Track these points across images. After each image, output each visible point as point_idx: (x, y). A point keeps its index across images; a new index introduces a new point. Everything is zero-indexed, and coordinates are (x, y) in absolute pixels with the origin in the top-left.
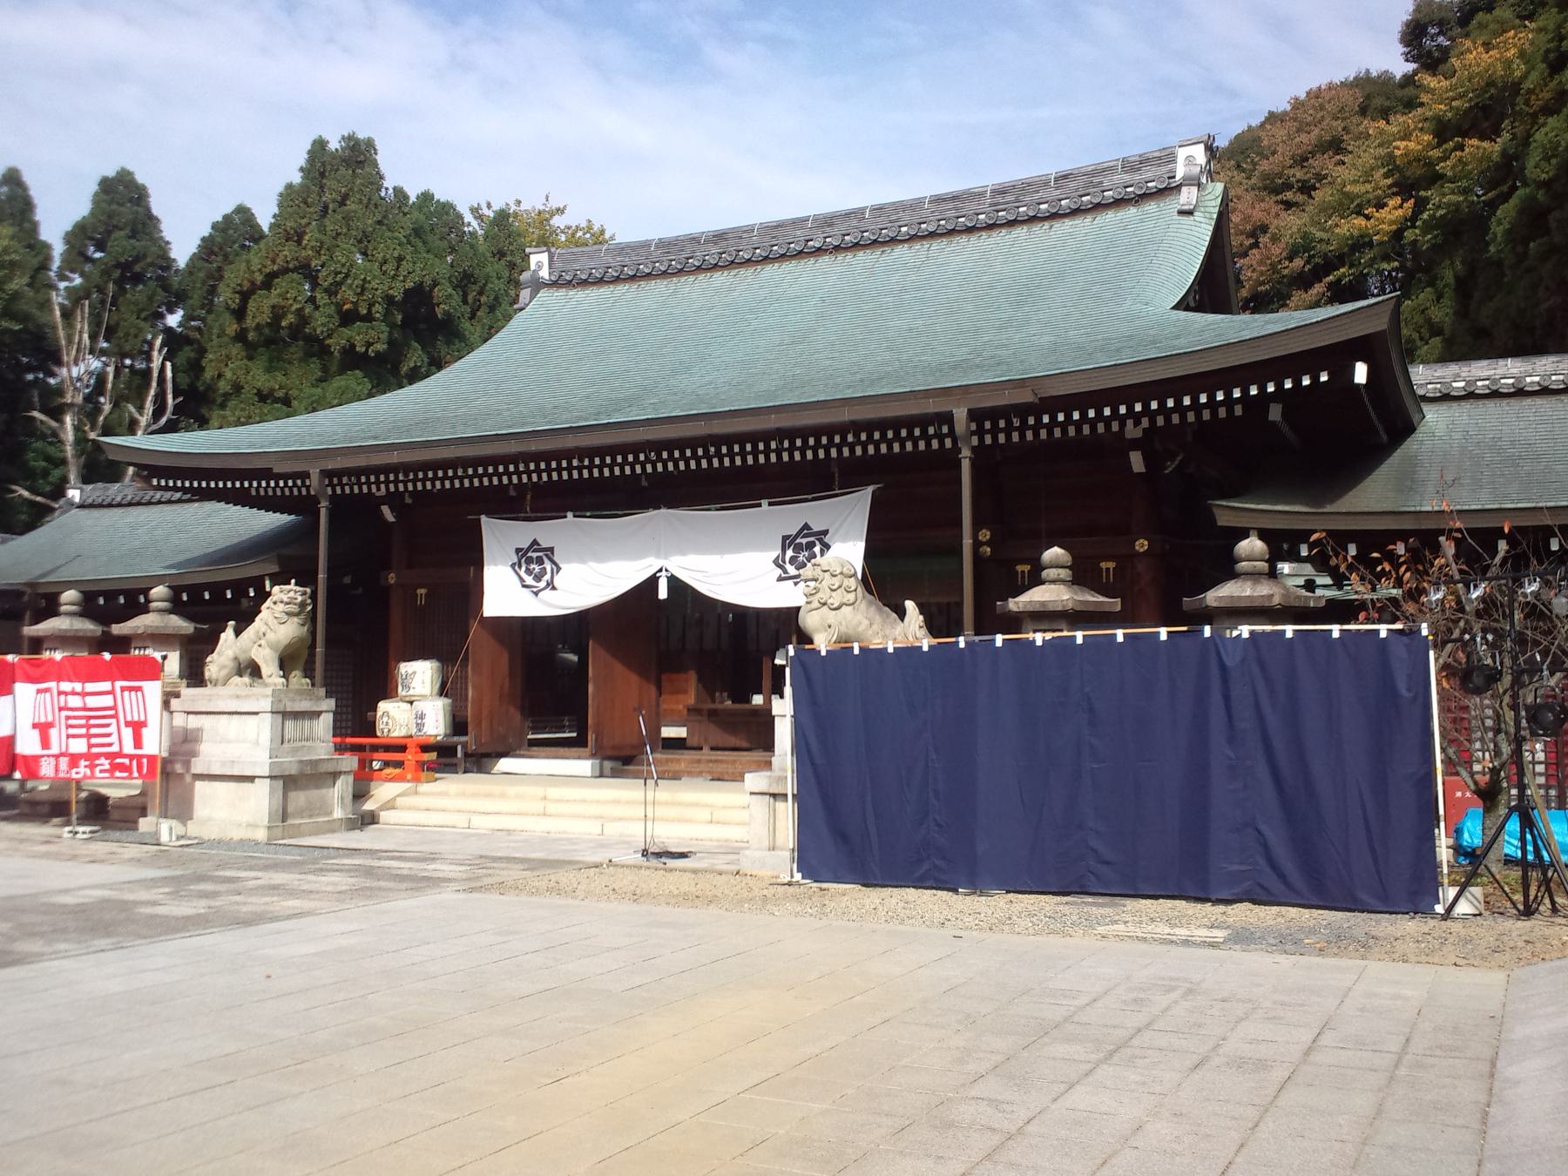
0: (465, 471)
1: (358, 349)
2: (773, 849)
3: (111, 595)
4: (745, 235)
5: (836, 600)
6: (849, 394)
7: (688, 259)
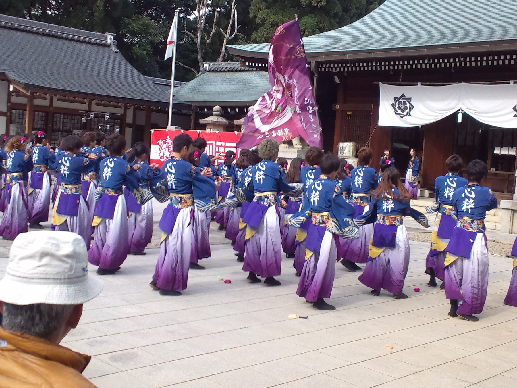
1: (313, 4)
2: (511, 233)
3: (233, 108)
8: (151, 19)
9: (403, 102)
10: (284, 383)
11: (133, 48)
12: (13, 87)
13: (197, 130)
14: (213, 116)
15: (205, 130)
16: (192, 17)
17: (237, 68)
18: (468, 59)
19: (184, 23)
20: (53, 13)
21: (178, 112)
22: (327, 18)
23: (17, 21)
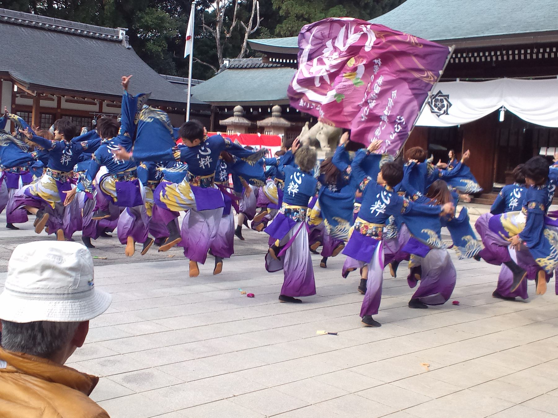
0: (468, 54)
3: (256, 108)
8: (165, 12)
9: (440, 99)
10: (312, 405)
11: (147, 44)
12: (18, 87)
13: (217, 132)
14: (233, 116)
15: (226, 132)
16: (210, 10)
17: (260, 65)
18: (510, 52)
19: (201, 16)
20: (60, 7)
21: (196, 113)
22: (357, 10)
23: (21, 16)
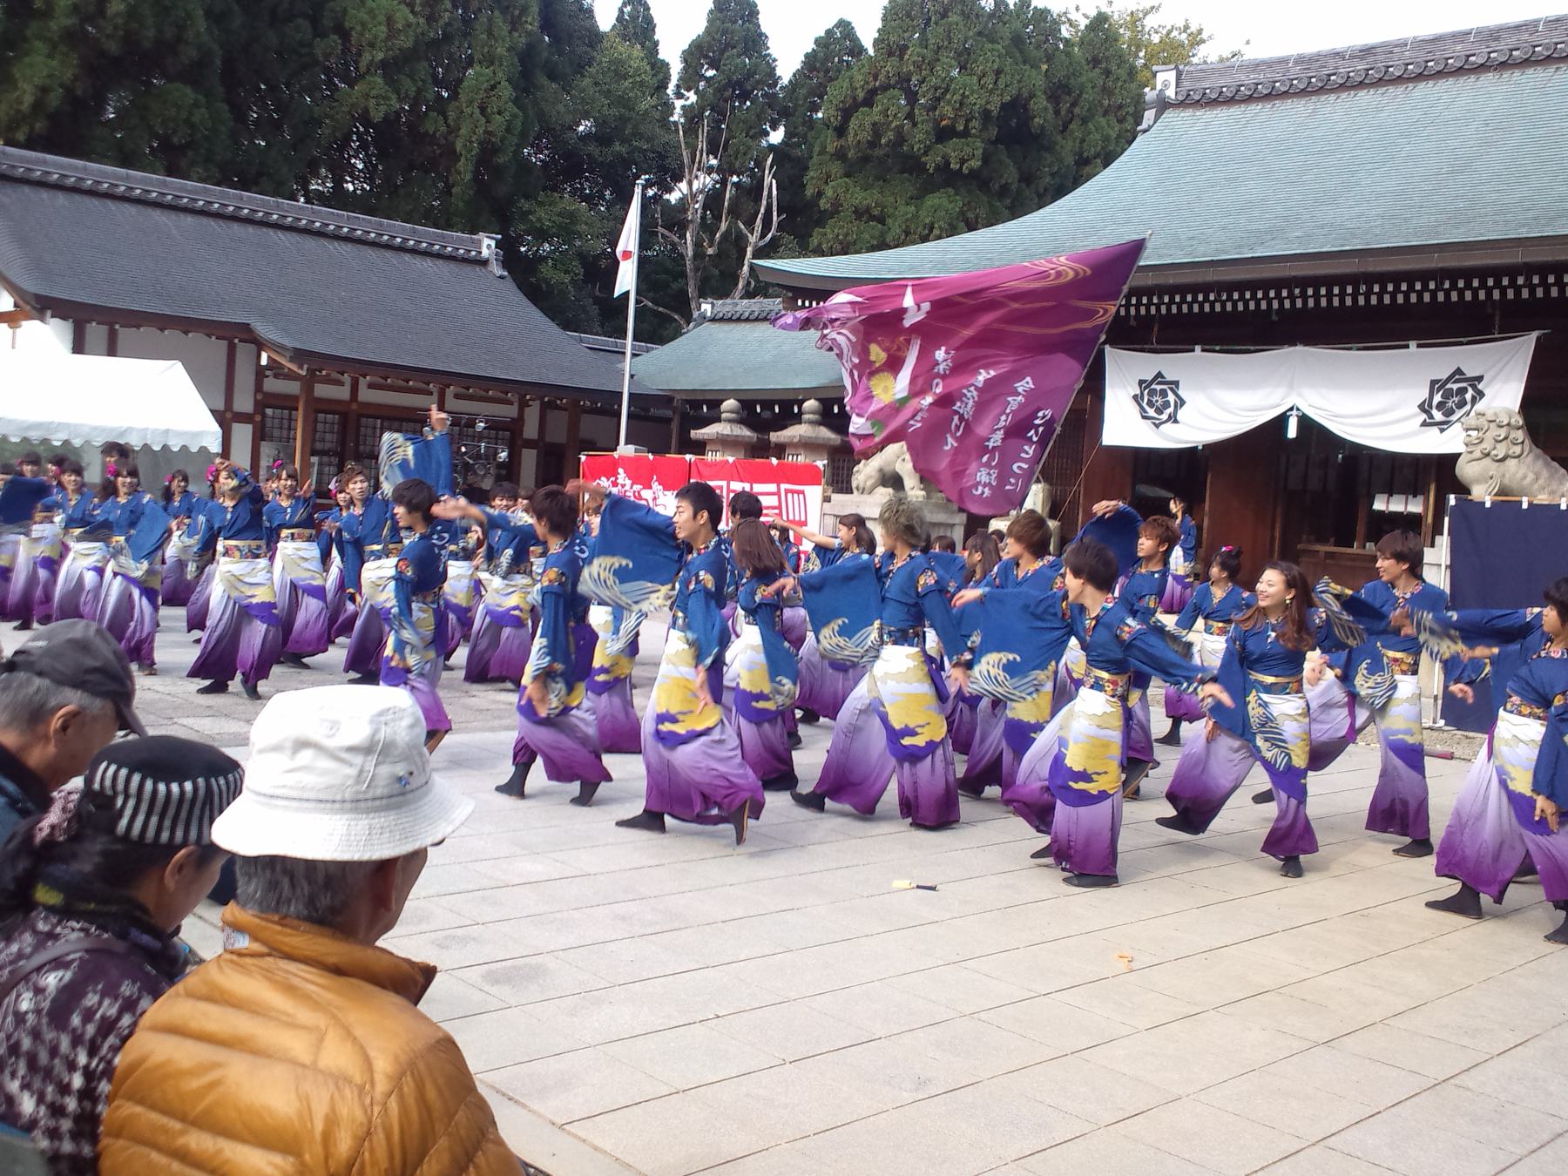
1: (952, 166)
3: (767, 404)
4: (1396, 50)
5: (1501, 451)
6: (1524, 233)
7: (1330, 75)
